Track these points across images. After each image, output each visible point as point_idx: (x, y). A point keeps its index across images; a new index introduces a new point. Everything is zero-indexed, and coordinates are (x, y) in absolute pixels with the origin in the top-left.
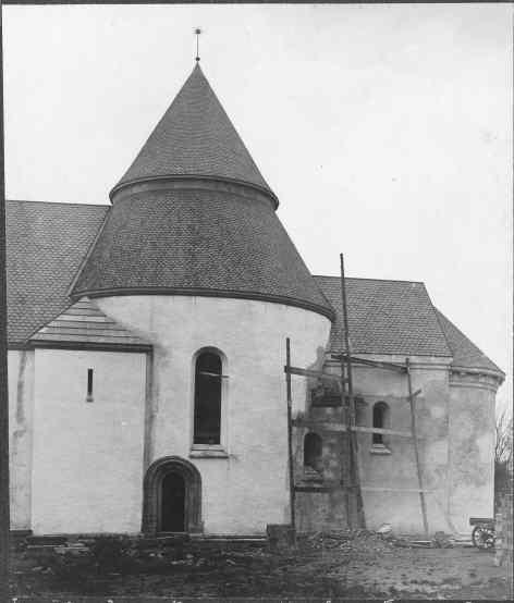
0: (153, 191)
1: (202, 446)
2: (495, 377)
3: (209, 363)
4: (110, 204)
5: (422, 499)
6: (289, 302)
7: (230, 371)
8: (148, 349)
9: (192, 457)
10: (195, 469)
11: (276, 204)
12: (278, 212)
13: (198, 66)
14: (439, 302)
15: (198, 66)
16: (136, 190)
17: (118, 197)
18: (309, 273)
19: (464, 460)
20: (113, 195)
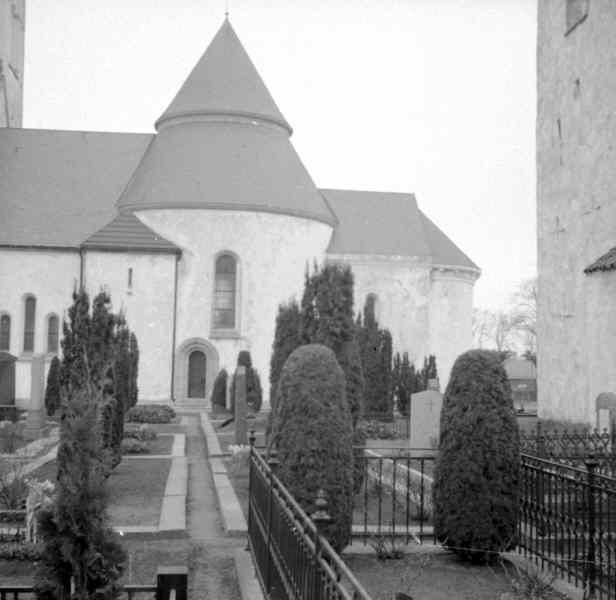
0: (183, 124)
1: (221, 330)
2: (471, 273)
3: (226, 265)
4: (156, 132)
5: (172, 396)
6: (276, 211)
7: (134, 271)
8: (178, 253)
9: (211, 338)
10: (214, 349)
11: (290, 132)
12: (293, 139)
13: (227, 20)
14: (421, 207)
15: (227, 20)
16: (173, 122)
17: (160, 127)
18: (313, 185)
19: (65, 374)
20: (157, 125)
